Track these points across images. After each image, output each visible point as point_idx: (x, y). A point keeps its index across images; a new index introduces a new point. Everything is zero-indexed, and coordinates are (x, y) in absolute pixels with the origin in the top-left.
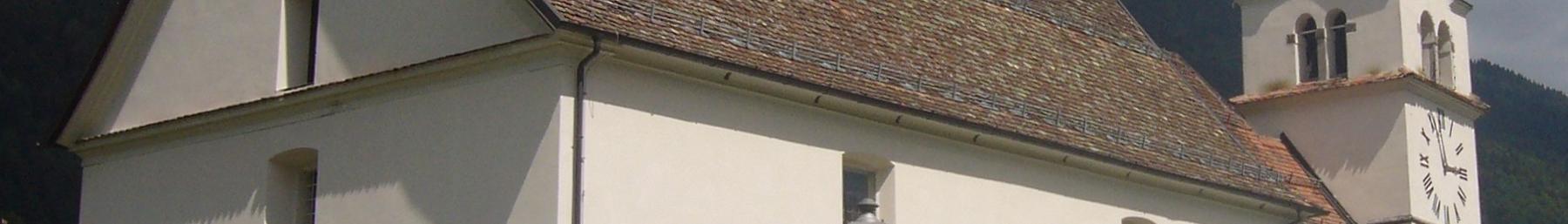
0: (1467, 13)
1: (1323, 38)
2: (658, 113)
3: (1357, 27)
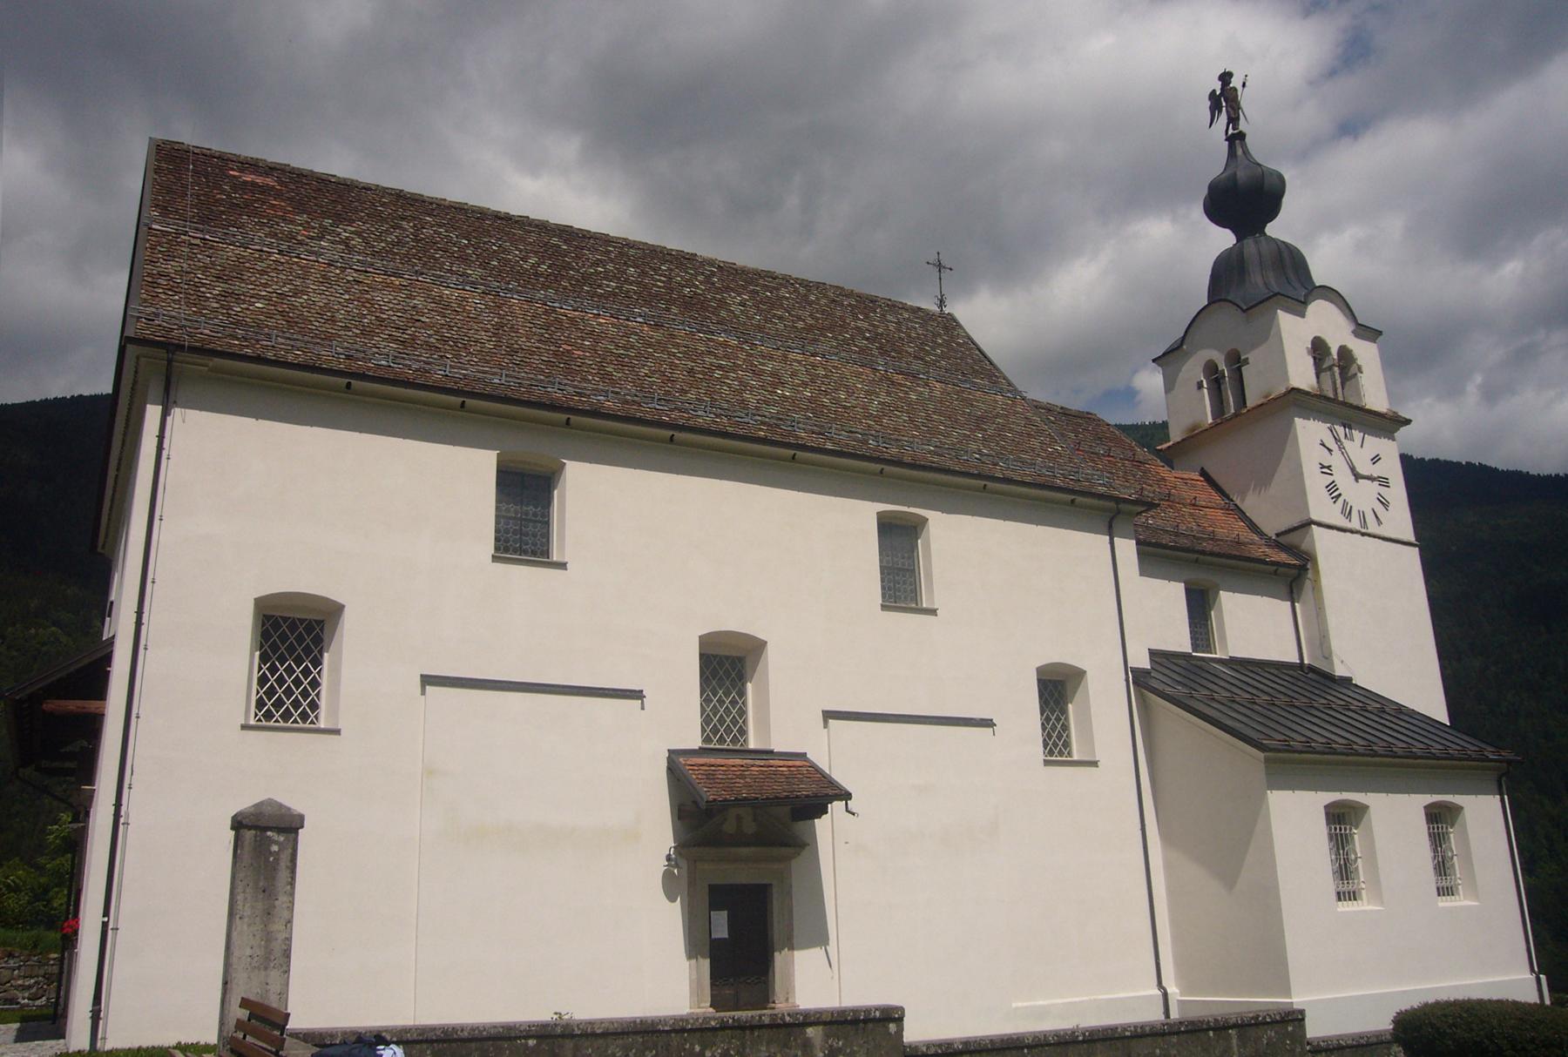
0: (1377, 339)
2: (1041, 525)
3: (1250, 361)
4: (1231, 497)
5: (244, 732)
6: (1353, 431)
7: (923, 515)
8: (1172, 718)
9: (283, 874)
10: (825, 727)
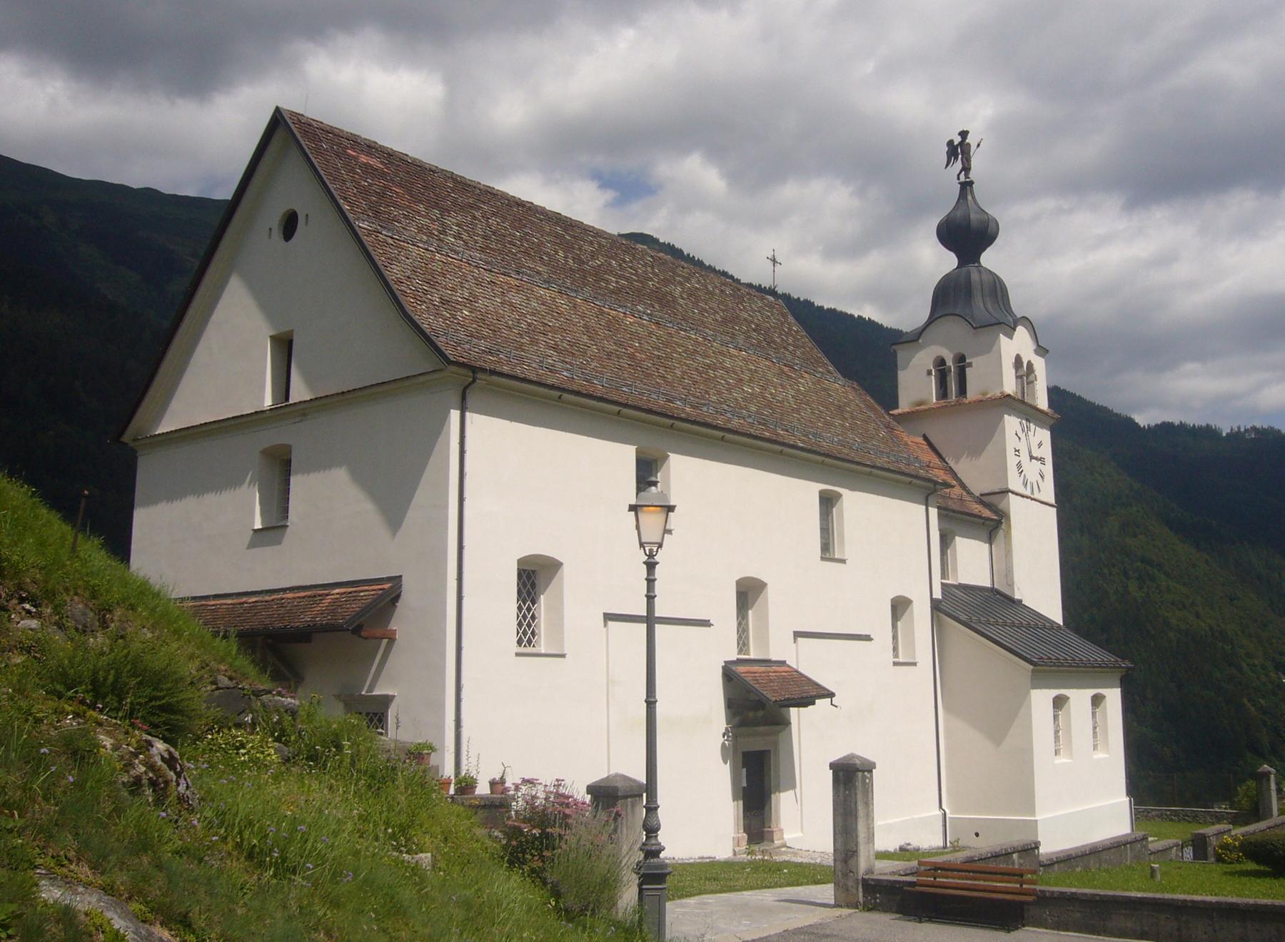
4: (946, 459)
5: (518, 658)
6: (1031, 424)
8: (957, 632)
9: (870, 794)
10: (795, 642)
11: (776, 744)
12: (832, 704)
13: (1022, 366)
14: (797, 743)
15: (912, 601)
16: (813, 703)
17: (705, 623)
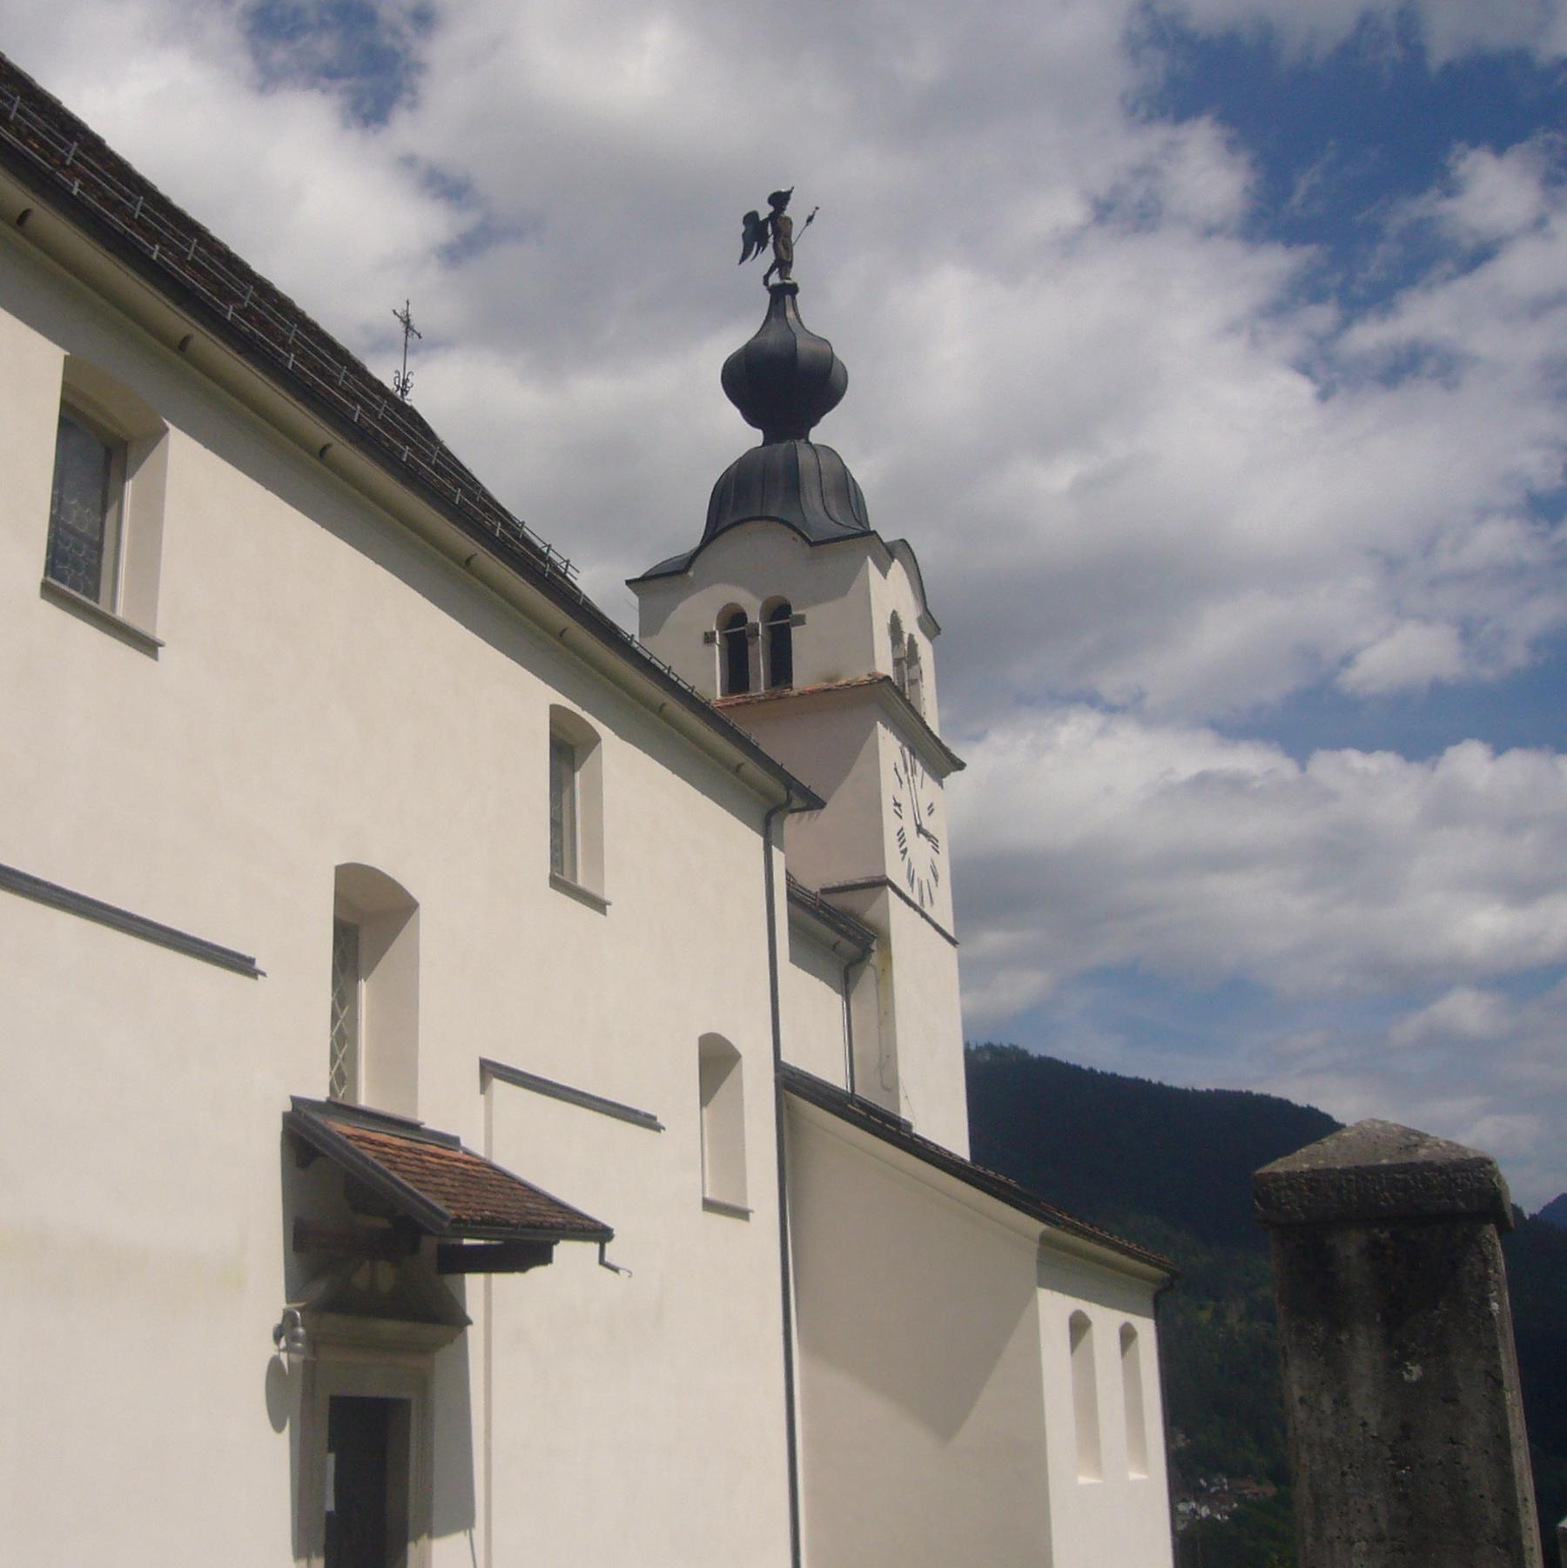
1: (758, 635)
3: (808, 620)
7: (598, 730)
11: (424, 1385)
12: (602, 1262)
13: (901, 640)
14: (482, 1386)
15: (740, 1056)
16: (544, 1257)
17: (243, 965)
